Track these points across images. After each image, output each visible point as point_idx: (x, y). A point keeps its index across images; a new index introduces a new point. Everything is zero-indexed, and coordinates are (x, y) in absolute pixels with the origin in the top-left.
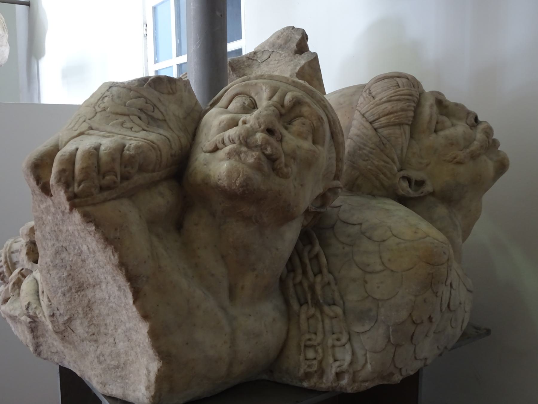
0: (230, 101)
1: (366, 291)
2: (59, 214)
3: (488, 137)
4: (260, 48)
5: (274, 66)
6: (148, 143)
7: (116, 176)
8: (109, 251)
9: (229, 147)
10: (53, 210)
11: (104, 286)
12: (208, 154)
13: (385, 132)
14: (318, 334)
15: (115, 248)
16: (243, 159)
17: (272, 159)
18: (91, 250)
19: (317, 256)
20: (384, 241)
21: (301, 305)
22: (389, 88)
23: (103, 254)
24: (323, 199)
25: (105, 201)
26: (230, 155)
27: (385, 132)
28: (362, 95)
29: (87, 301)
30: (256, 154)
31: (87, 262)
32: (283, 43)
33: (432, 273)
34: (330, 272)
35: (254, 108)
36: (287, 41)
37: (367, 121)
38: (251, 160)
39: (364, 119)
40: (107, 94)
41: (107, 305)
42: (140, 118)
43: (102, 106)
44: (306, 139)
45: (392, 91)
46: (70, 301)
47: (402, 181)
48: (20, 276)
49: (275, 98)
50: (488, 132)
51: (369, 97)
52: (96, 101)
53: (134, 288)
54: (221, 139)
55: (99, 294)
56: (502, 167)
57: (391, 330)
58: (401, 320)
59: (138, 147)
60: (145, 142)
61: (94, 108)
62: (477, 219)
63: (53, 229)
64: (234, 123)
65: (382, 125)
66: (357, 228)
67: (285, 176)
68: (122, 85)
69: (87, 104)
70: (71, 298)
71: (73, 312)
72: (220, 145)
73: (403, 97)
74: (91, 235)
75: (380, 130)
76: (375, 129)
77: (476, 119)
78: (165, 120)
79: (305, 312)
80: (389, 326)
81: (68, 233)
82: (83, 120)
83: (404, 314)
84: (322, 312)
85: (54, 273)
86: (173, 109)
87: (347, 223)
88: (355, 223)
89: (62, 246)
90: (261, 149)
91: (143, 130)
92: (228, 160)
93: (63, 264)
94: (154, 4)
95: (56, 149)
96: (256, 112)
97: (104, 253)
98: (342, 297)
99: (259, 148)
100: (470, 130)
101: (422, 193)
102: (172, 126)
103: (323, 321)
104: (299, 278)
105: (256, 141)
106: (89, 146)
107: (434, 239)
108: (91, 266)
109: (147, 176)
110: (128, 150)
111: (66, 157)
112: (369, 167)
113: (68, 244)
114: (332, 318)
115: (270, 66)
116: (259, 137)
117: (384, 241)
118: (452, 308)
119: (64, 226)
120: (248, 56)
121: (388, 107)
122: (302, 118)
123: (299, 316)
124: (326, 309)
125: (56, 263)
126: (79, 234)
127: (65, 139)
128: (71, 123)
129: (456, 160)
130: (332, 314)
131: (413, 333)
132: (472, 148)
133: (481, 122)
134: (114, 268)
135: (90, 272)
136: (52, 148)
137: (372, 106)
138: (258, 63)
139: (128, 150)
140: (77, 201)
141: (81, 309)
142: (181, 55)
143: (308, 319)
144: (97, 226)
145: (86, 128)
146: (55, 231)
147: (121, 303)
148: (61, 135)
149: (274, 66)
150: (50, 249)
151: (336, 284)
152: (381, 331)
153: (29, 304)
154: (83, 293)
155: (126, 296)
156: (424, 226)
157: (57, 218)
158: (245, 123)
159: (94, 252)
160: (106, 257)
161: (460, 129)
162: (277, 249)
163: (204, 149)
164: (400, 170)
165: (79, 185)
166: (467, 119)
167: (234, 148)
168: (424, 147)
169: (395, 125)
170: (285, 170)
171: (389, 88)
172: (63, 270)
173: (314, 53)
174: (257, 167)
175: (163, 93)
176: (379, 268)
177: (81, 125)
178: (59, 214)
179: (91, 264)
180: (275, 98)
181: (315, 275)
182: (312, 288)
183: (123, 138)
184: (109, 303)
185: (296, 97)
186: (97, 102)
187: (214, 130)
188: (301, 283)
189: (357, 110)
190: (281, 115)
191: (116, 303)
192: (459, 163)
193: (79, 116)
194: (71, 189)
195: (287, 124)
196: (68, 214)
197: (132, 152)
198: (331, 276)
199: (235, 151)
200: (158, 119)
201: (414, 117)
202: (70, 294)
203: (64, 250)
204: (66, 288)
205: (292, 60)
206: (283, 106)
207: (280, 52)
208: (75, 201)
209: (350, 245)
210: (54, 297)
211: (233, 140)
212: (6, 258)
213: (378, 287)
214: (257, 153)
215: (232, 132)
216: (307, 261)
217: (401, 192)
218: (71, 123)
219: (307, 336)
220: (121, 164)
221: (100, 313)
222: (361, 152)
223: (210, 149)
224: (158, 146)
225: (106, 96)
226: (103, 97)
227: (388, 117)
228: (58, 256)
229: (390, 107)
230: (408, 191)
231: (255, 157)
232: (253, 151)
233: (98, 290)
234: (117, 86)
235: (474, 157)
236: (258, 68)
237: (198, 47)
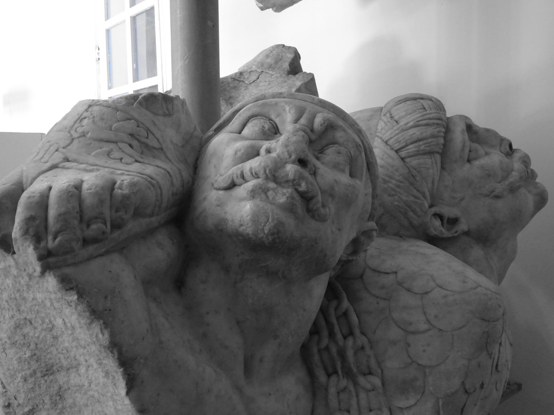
0: (244, 126)
1: (409, 356)
2: (23, 278)
3: (526, 167)
4: (245, 68)
5: (264, 88)
6: (146, 180)
7: (105, 224)
8: (96, 327)
9: (251, 184)
10: (14, 271)
11: (82, 370)
12: (221, 192)
13: (414, 162)
14: (352, 412)
15: (104, 323)
16: (271, 198)
17: (306, 198)
18: (69, 325)
19: (346, 314)
20: (427, 293)
21: (329, 376)
22: (415, 111)
23: (87, 331)
24: (356, 246)
25: (91, 258)
26: (253, 194)
27: (414, 162)
28: (381, 119)
29: (56, 388)
30: (288, 191)
31: (60, 339)
32: (272, 62)
33: (488, 332)
34: (363, 333)
35: (276, 134)
36: (278, 60)
37: (392, 149)
38: (282, 200)
39: (388, 147)
40: (86, 114)
41: (86, 393)
42: (131, 146)
43: (80, 130)
44: (343, 171)
45: (419, 115)
46: (32, 388)
47: (434, 220)
49: (303, 121)
50: (526, 161)
51: (392, 121)
52: (72, 124)
53: (129, 375)
54: (239, 173)
55: (74, 379)
56: (542, 200)
57: (441, 403)
58: (453, 390)
59: (133, 185)
60: (143, 178)
61: (69, 132)
62: (512, 260)
63: (13, 296)
64: (254, 153)
65: (411, 154)
66: (392, 277)
67: (322, 219)
68: (105, 104)
69: (57, 128)
70: (35, 384)
71: (37, 402)
72: (238, 181)
73: (432, 121)
74: (71, 306)
75: (408, 160)
76: (403, 159)
77: (510, 146)
78: (162, 149)
79: (335, 384)
80: (438, 399)
81: (34, 302)
82: (56, 148)
83: (456, 382)
84: (356, 384)
85: (11, 352)
86: (169, 136)
87: (379, 272)
88: (388, 271)
89: (26, 319)
90: (294, 185)
91: (136, 161)
92: (250, 200)
93: (25, 342)
94: (107, 27)
95: (18, 189)
96: (282, 139)
97: (88, 330)
98: (379, 364)
99: (291, 184)
100: (506, 160)
101: (456, 232)
102: (170, 156)
103: (357, 396)
104: (325, 341)
105: (287, 175)
106: (66, 185)
107: (486, 289)
108: (66, 344)
109: (144, 222)
110: (120, 188)
111: (36, 199)
112: (396, 203)
113: (34, 316)
114: (368, 391)
115: (260, 88)
116: (291, 169)
117: (427, 293)
118: (500, 368)
119: (30, 292)
120: (234, 76)
121: (416, 132)
122: (337, 145)
123: (326, 389)
124: (362, 380)
125: (16, 340)
126: (52, 304)
127: (32, 173)
128: (38, 153)
129: (493, 194)
130: (369, 386)
131: (464, 405)
132: (511, 180)
133: (516, 150)
134: (103, 350)
135: (64, 351)
136: (13, 187)
137: (397, 131)
138: (245, 85)
139: (120, 188)
140: (51, 260)
141: (48, 398)
142: (138, 81)
143: (338, 393)
144: (80, 295)
145: (61, 160)
146: (15, 299)
147: (107, 392)
148: (25, 168)
149: (264, 88)
150: (7, 322)
151: (371, 348)
152: (430, 404)
154: (51, 377)
155: (115, 385)
156: (472, 274)
157: (20, 282)
158: (268, 151)
159: (73, 328)
160: (91, 335)
161: (495, 158)
162: (305, 310)
163: (215, 186)
164: (431, 206)
165: (55, 238)
166: (500, 146)
167: (259, 184)
168: (440, 179)
169: (425, 153)
170: (322, 211)
171: (415, 111)
172: (25, 349)
173: (310, 73)
174: (289, 208)
176: (423, 326)
177: (52, 155)
178: (23, 278)
179: (66, 341)
180: (303, 121)
181: (345, 338)
182: (342, 353)
183: (112, 173)
184: (89, 391)
185: (328, 120)
186: (73, 125)
187: (227, 160)
188: (327, 348)
189: (377, 136)
190: (311, 142)
191: (100, 392)
192: (497, 197)
193: (48, 144)
194: (43, 244)
195: (319, 153)
196: (38, 278)
197: (126, 191)
198: (364, 339)
199: (260, 188)
200: (153, 148)
201: (444, 145)
202: (33, 379)
203: (28, 323)
204: (28, 372)
205: (285, 82)
206: (312, 130)
207: (271, 72)
208: (49, 260)
209: (385, 299)
210: (11, 382)
211: (256, 174)
214: (290, 190)
215: (254, 163)
216: (334, 321)
217: (433, 232)
218: (38, 153)
220: (111, 207)
221: (74, 404)
222: (385, 186)
223: (224, 185)
224: (158, 183)
225: (85, 118)
226: (80, 119)
227: (416, 144)
228: (18, 331)
229: (418, 133)
230: (441, 231)
231: (287, 195)
232: (283, 187)
233: (73, 375)
234: (99, 105)
235: (513, 190)
236: (245, 90)
237: (187, 62)
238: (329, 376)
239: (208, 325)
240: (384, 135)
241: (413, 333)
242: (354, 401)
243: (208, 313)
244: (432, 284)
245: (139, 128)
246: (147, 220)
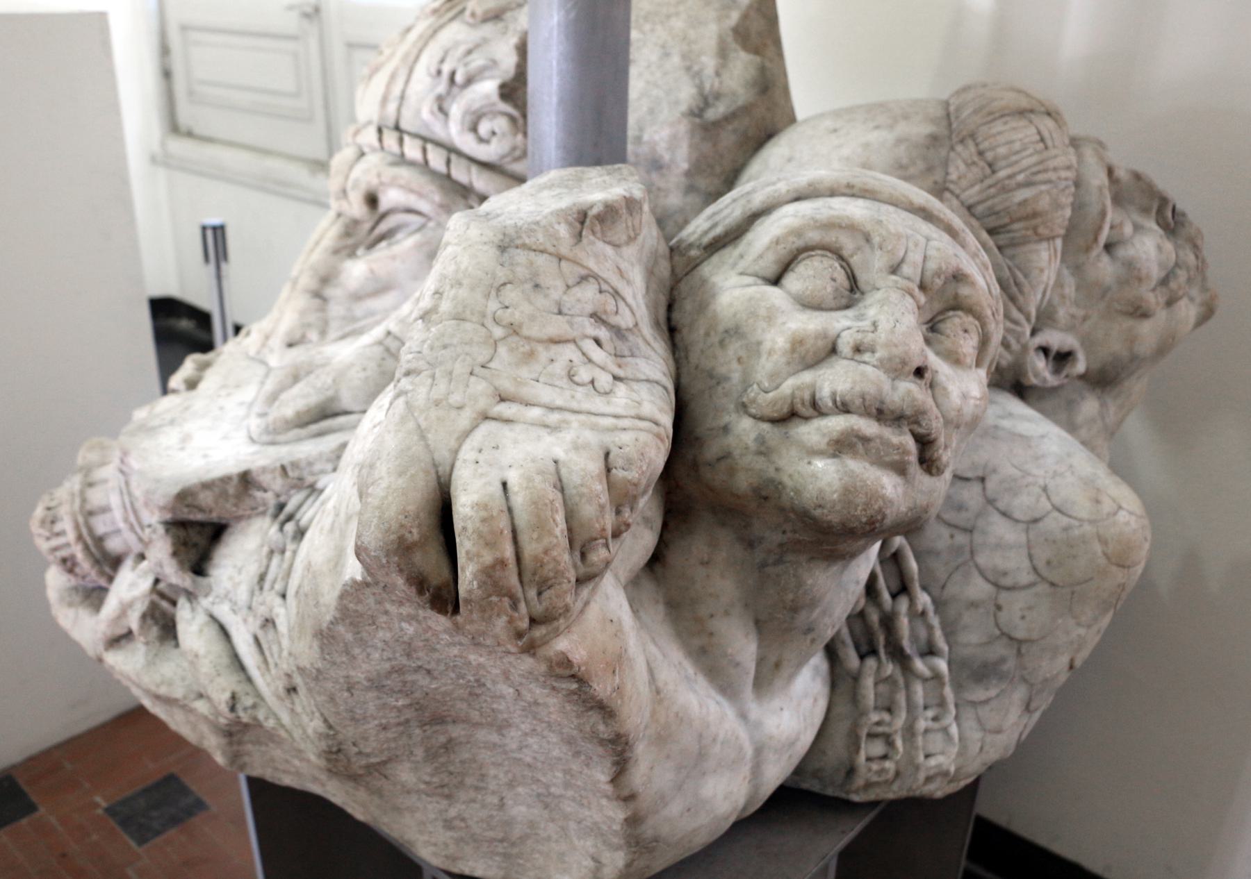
1: (997, 625)
42: (598, 342)
48: (155, 597)
54: (807, 396)
124: (919, 665)
153: (234, 697)
176: (1025, 577)
212: (77, 527)
213: (1023, 617)
219: (875, 717)
237: (572, 15)
238: (862, 657)
239: (711, 634)
240: (964, 191)
241: (1008, 589)
242: (901, 698)
243: (712, 616)
244: (1045, 505)
245: (603, 296)
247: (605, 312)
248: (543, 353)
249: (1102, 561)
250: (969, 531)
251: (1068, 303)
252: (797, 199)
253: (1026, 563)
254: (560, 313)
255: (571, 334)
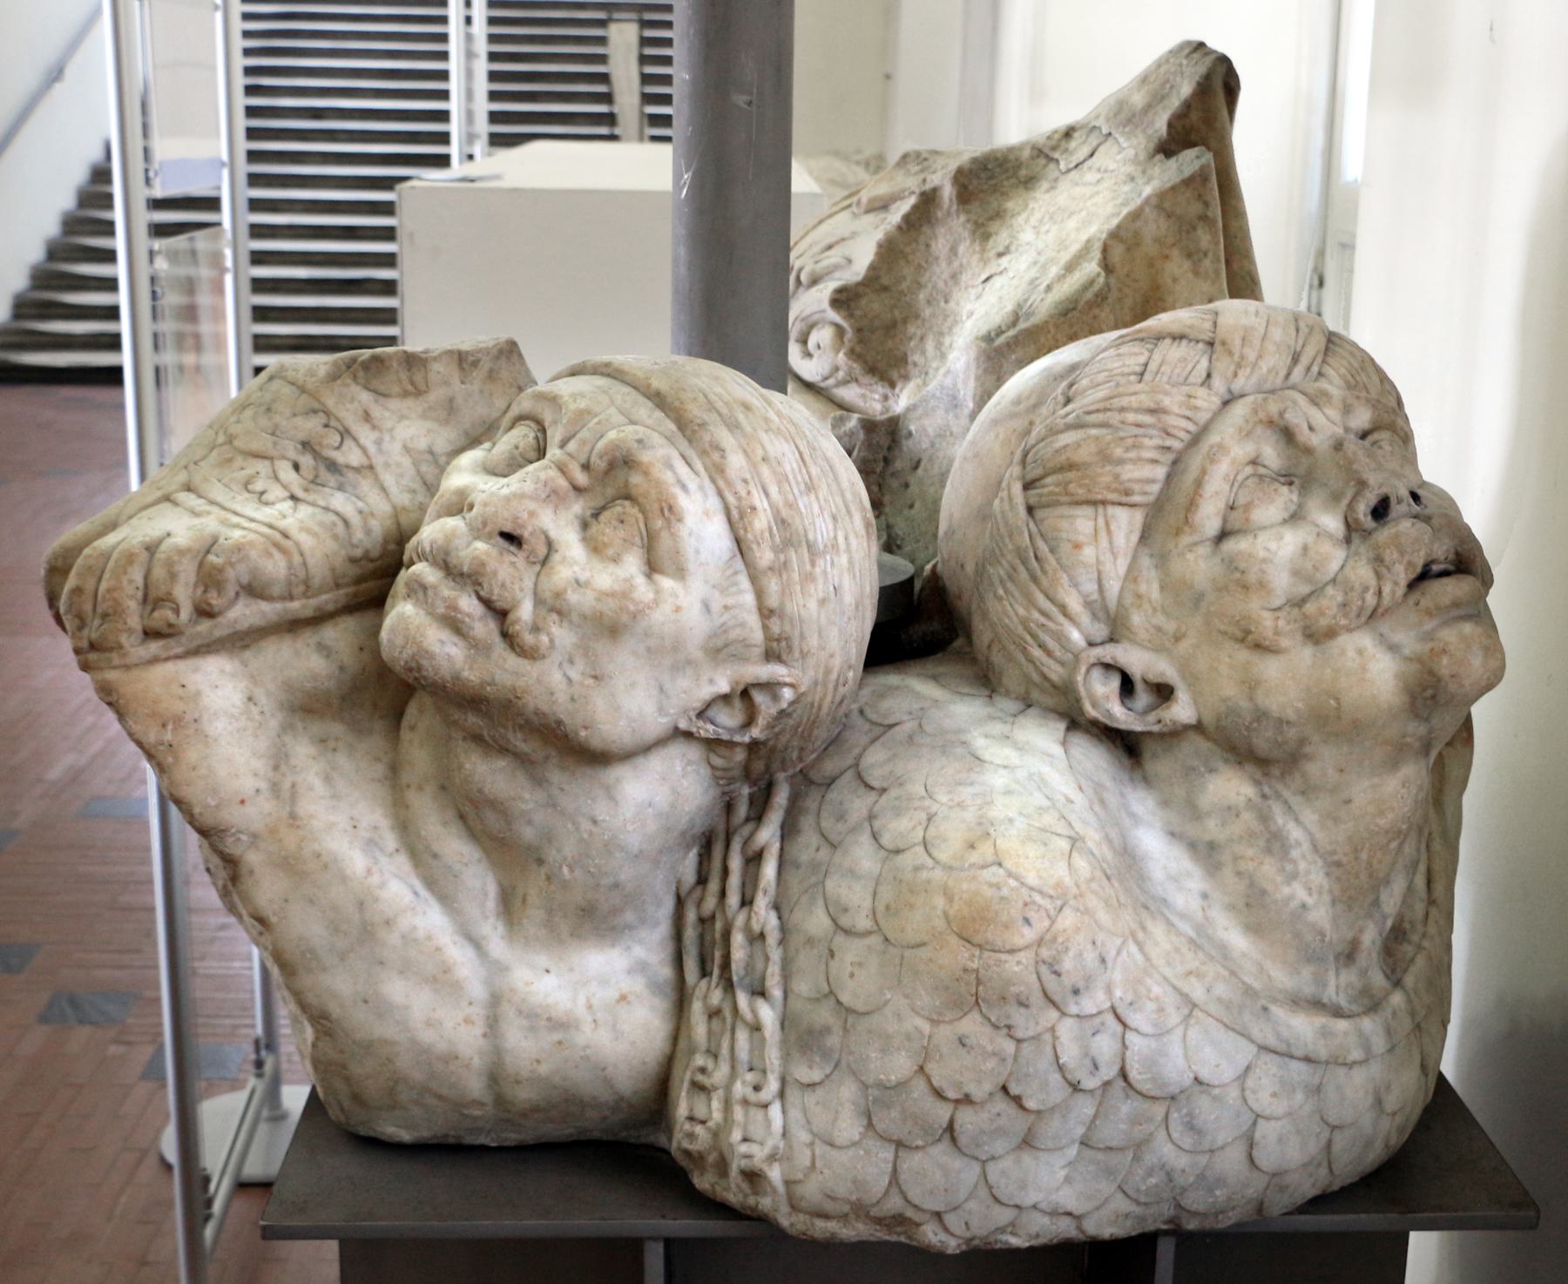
25: (155, 660)
42: (296, 467)
47: (1097, 673)
109: (266, 611)
162: (595, 822)
175: (385, 396)
176: (863, 923)
242: (725, 1045)
246: (278, 606)
247: (320, 444)
248: (239, 461)
249: (940, 924)
250: (834, 846)
251: (1146, 606)
252: (573, 374)
253: (867, 904)
254: (273, 434)
255: (272, 452)
